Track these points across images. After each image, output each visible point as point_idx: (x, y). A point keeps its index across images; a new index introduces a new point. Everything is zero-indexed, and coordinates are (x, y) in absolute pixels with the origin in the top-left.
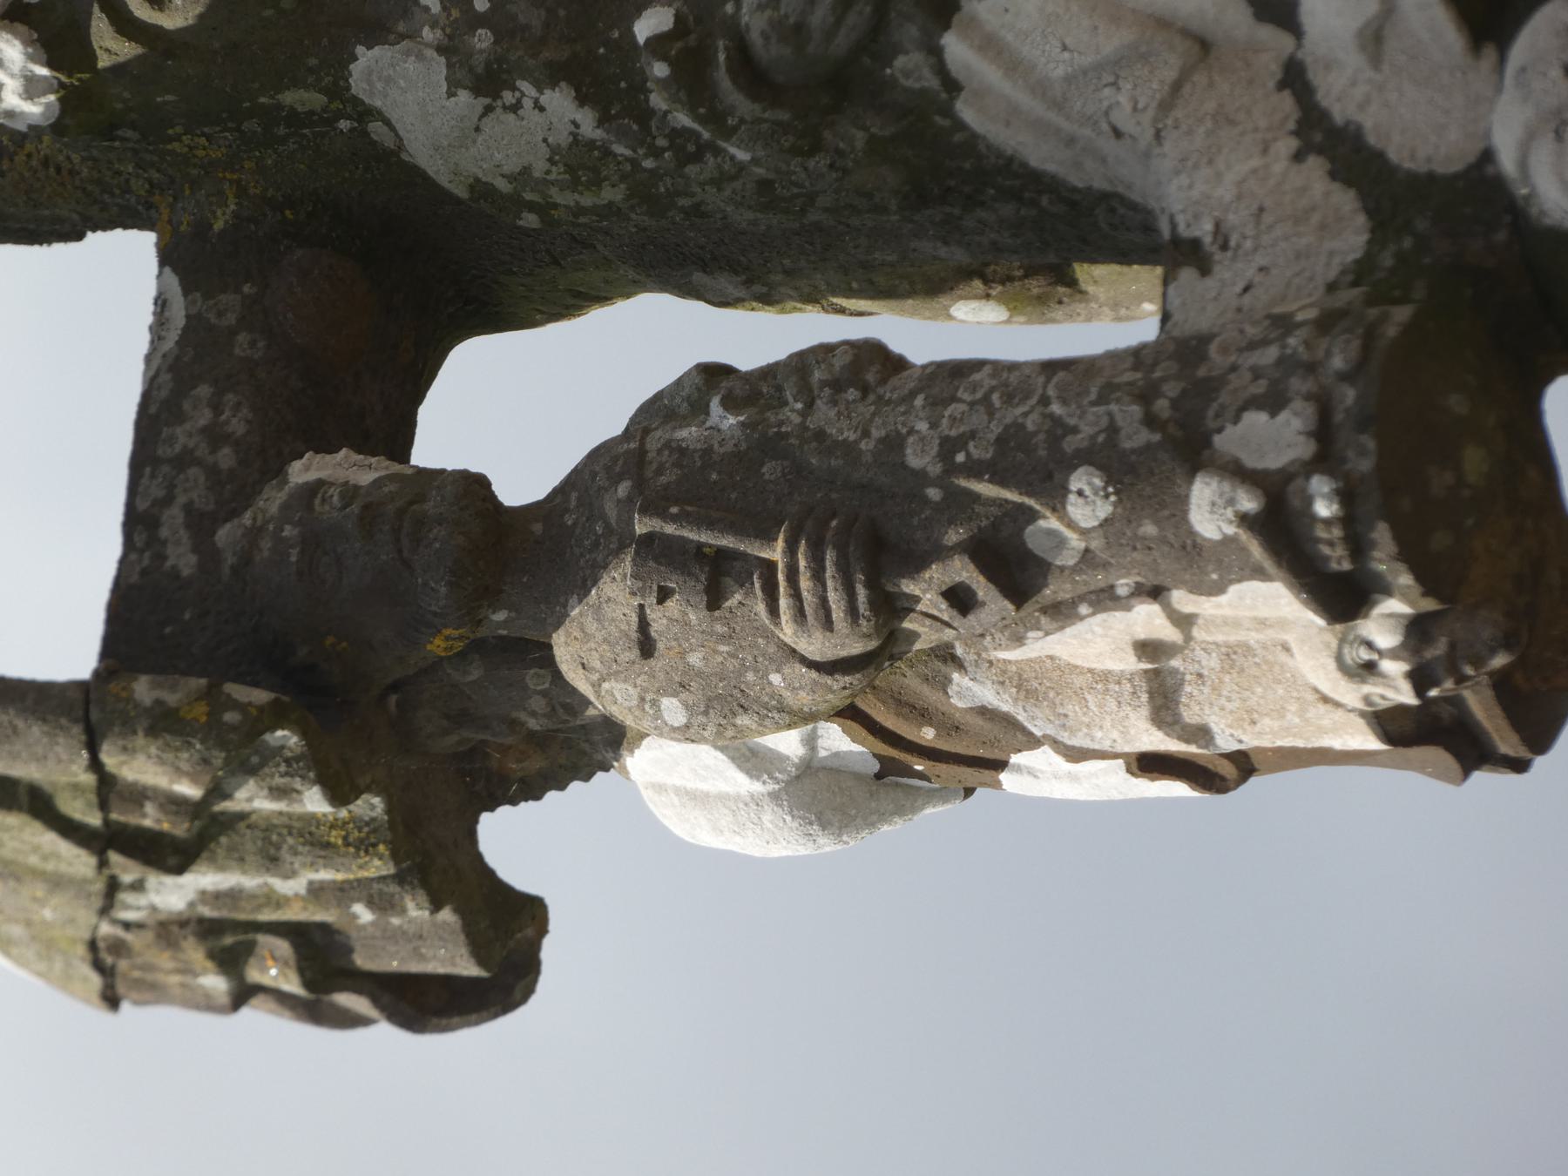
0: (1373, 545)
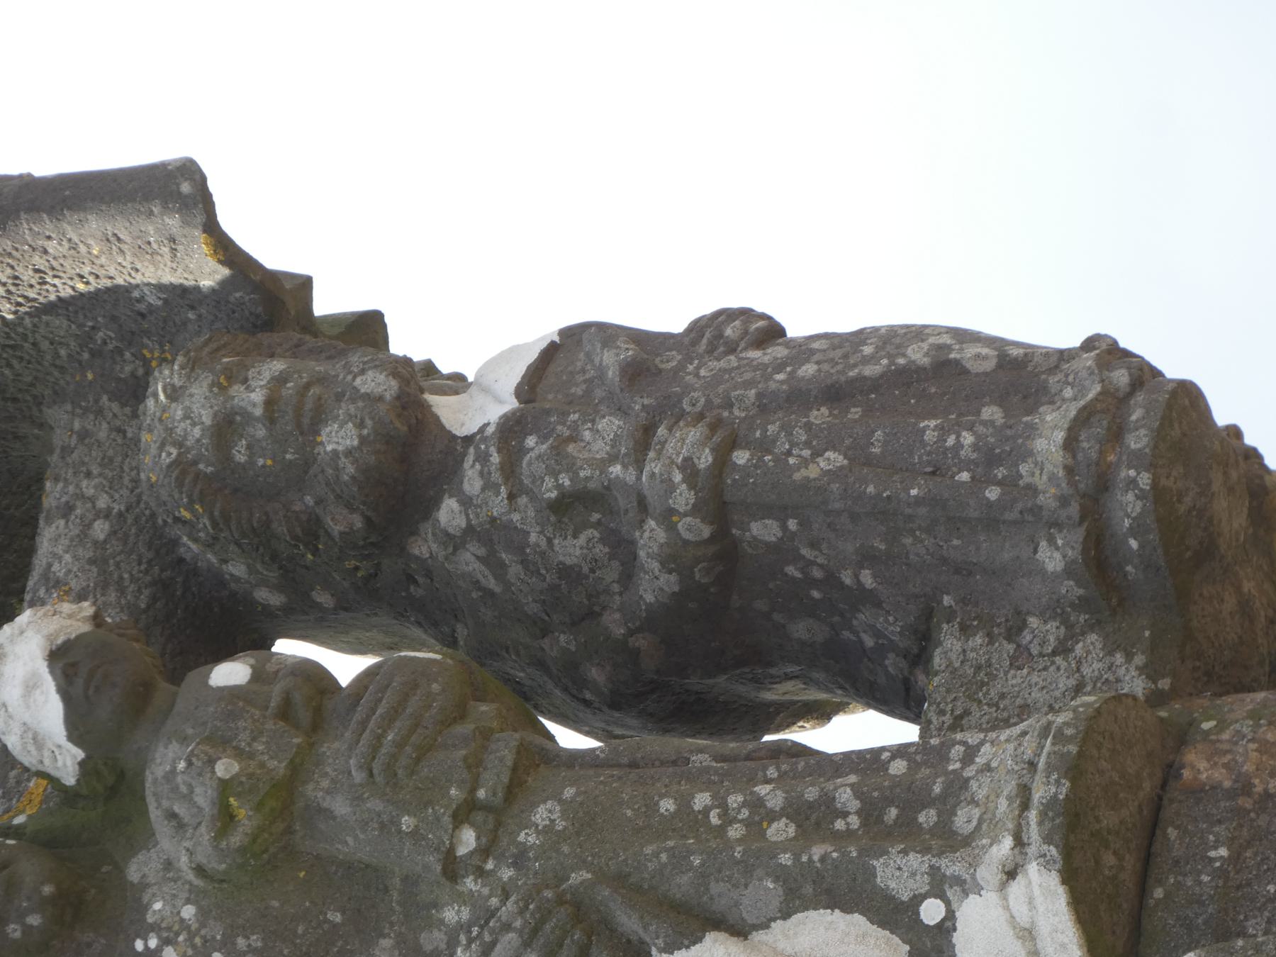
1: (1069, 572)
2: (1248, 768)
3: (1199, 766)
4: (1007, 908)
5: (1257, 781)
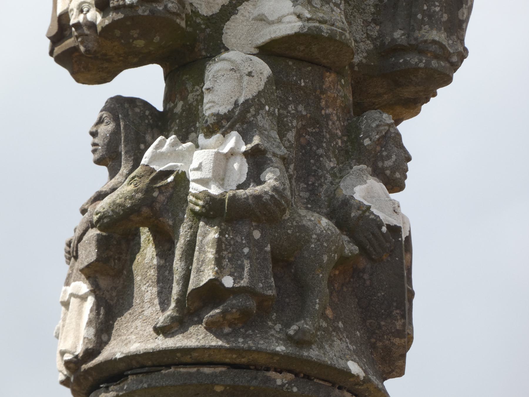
0: (117, 13)
1: (393, 40)
3: (330, 78)
5: (325, 96)
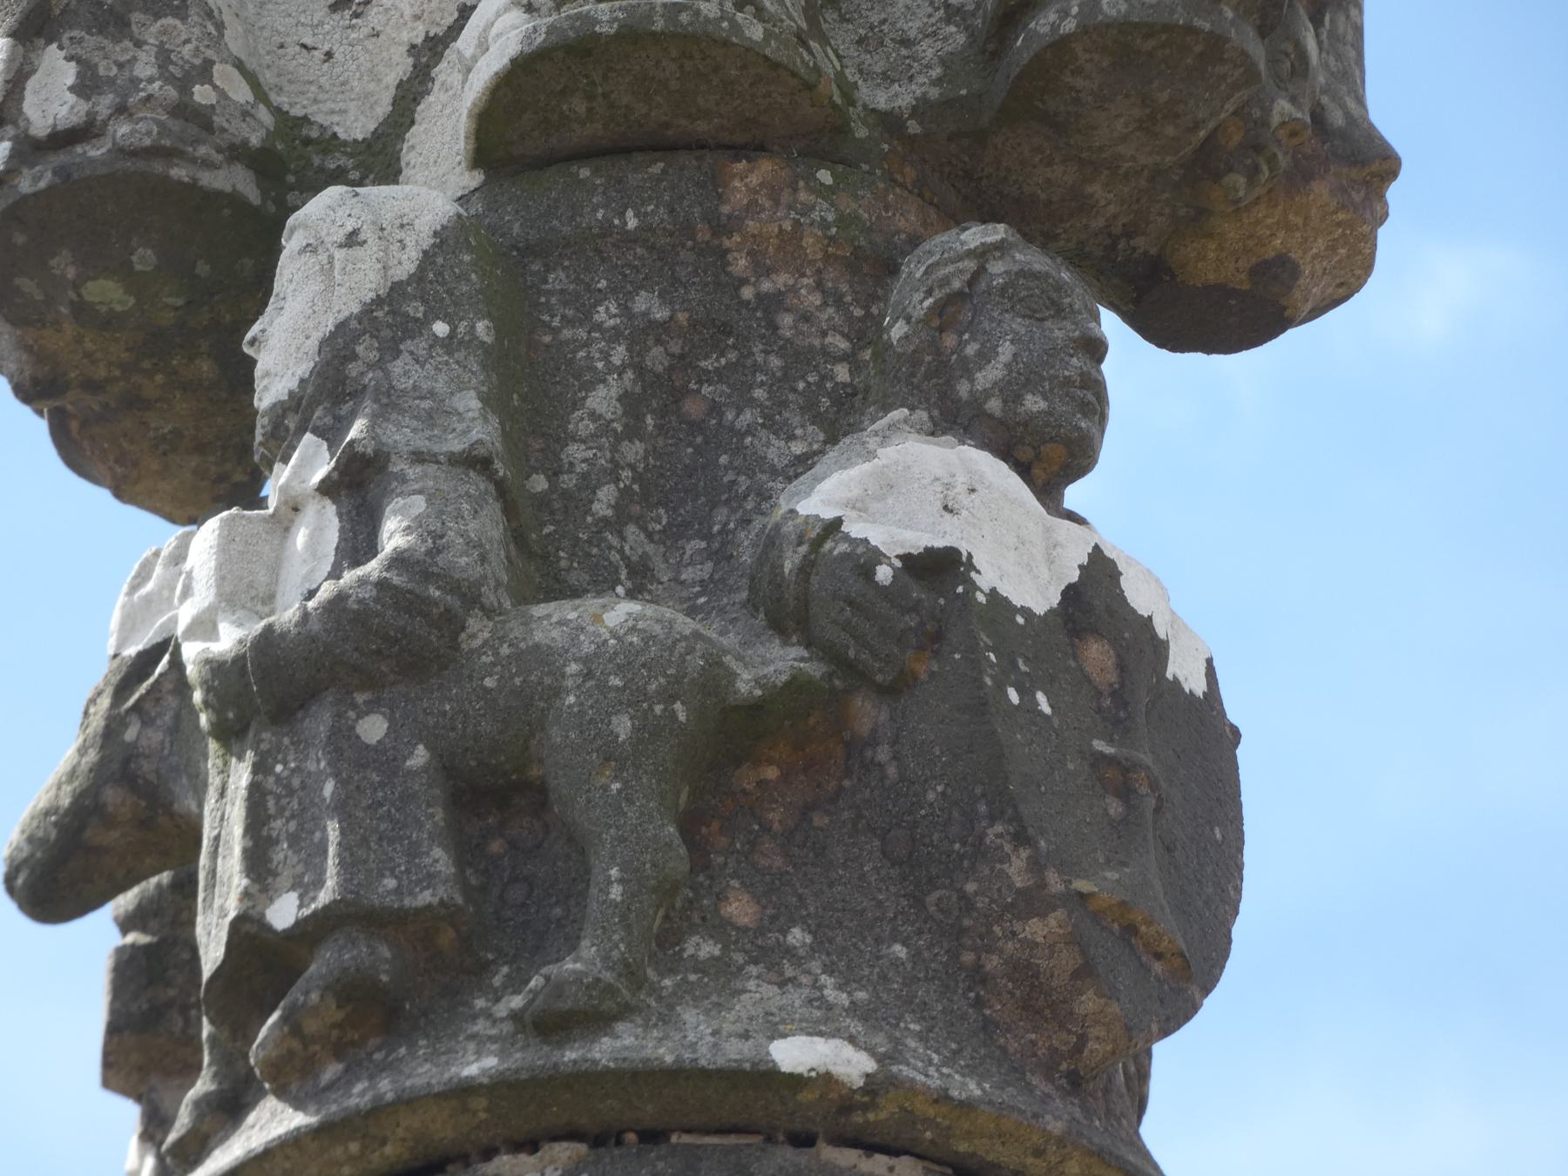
2: (752, 225)
3: (747, 180)
4: (498, 15)
5: (737, 238)
